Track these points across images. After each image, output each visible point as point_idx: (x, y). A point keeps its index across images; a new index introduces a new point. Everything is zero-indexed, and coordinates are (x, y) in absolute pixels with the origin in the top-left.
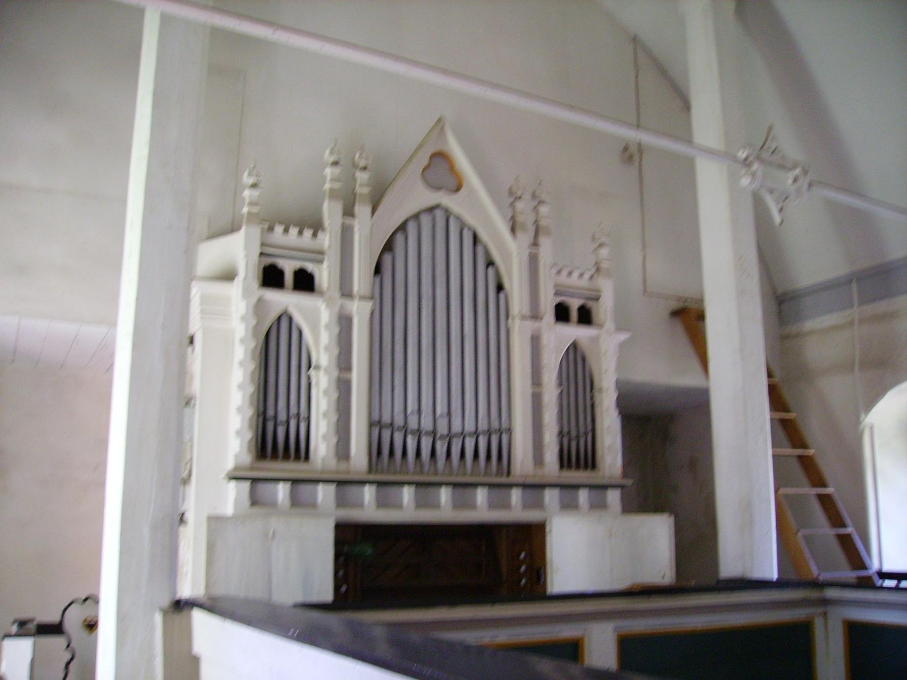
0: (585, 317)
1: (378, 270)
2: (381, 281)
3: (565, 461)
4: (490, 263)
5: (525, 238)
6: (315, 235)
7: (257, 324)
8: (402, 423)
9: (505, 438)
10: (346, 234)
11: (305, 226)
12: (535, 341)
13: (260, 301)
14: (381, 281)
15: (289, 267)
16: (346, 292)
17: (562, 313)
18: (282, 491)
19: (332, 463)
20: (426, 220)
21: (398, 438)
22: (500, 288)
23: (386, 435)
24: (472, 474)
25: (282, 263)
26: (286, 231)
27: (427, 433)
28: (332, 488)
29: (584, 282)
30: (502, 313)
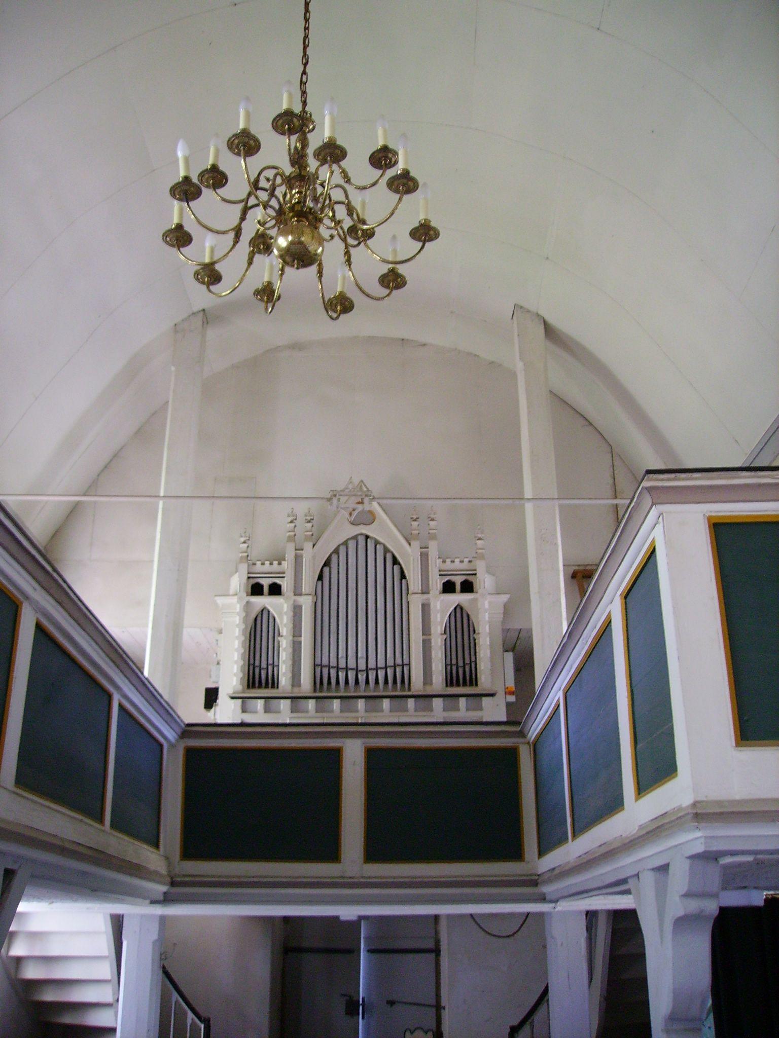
0: (468, 587)
1: (320, 578)
2: (322, 584)
3: (451, 681)
4: (395, 561)
5: (416, 544)
6: (280, 564)
7: (247, 616)
8: (335, 665)
9: (275, 669)
10: (298, 559)
11: (509, 593)
12: (426, 608)
13: (248, 602)
14: (322, 584)
15: (266, 583)
16: (297, 592)
17: (448, 588)
18: (260, 704)
19: (289, 688)
20: (352, 545)
21: (333, 672)
22: (403, 576)
23: (325, 671)
24: (365, 691)
25: (262, 581)
26: (271, 564)
27: (454, 665)
28: (288, 701)
29: (465, 565)
30: (404, 591)
